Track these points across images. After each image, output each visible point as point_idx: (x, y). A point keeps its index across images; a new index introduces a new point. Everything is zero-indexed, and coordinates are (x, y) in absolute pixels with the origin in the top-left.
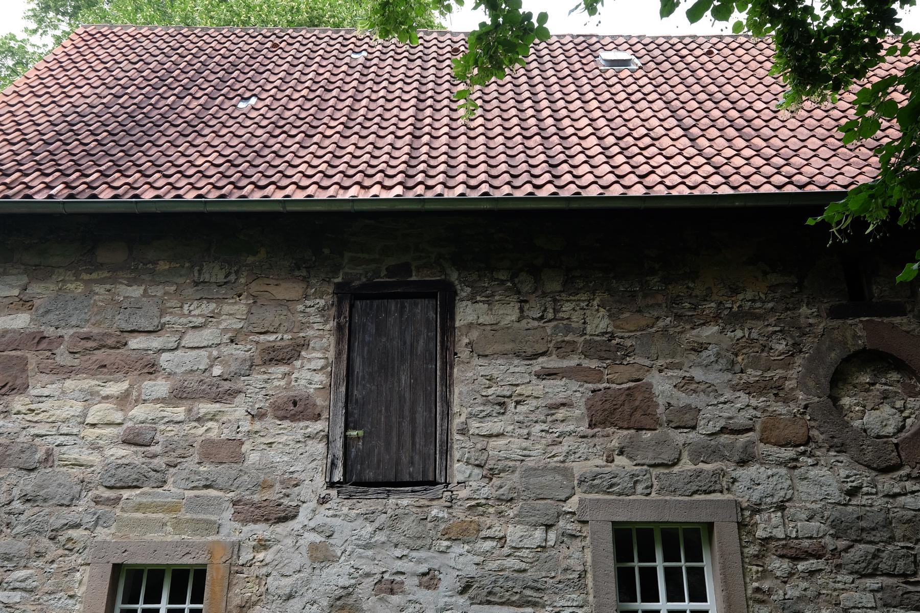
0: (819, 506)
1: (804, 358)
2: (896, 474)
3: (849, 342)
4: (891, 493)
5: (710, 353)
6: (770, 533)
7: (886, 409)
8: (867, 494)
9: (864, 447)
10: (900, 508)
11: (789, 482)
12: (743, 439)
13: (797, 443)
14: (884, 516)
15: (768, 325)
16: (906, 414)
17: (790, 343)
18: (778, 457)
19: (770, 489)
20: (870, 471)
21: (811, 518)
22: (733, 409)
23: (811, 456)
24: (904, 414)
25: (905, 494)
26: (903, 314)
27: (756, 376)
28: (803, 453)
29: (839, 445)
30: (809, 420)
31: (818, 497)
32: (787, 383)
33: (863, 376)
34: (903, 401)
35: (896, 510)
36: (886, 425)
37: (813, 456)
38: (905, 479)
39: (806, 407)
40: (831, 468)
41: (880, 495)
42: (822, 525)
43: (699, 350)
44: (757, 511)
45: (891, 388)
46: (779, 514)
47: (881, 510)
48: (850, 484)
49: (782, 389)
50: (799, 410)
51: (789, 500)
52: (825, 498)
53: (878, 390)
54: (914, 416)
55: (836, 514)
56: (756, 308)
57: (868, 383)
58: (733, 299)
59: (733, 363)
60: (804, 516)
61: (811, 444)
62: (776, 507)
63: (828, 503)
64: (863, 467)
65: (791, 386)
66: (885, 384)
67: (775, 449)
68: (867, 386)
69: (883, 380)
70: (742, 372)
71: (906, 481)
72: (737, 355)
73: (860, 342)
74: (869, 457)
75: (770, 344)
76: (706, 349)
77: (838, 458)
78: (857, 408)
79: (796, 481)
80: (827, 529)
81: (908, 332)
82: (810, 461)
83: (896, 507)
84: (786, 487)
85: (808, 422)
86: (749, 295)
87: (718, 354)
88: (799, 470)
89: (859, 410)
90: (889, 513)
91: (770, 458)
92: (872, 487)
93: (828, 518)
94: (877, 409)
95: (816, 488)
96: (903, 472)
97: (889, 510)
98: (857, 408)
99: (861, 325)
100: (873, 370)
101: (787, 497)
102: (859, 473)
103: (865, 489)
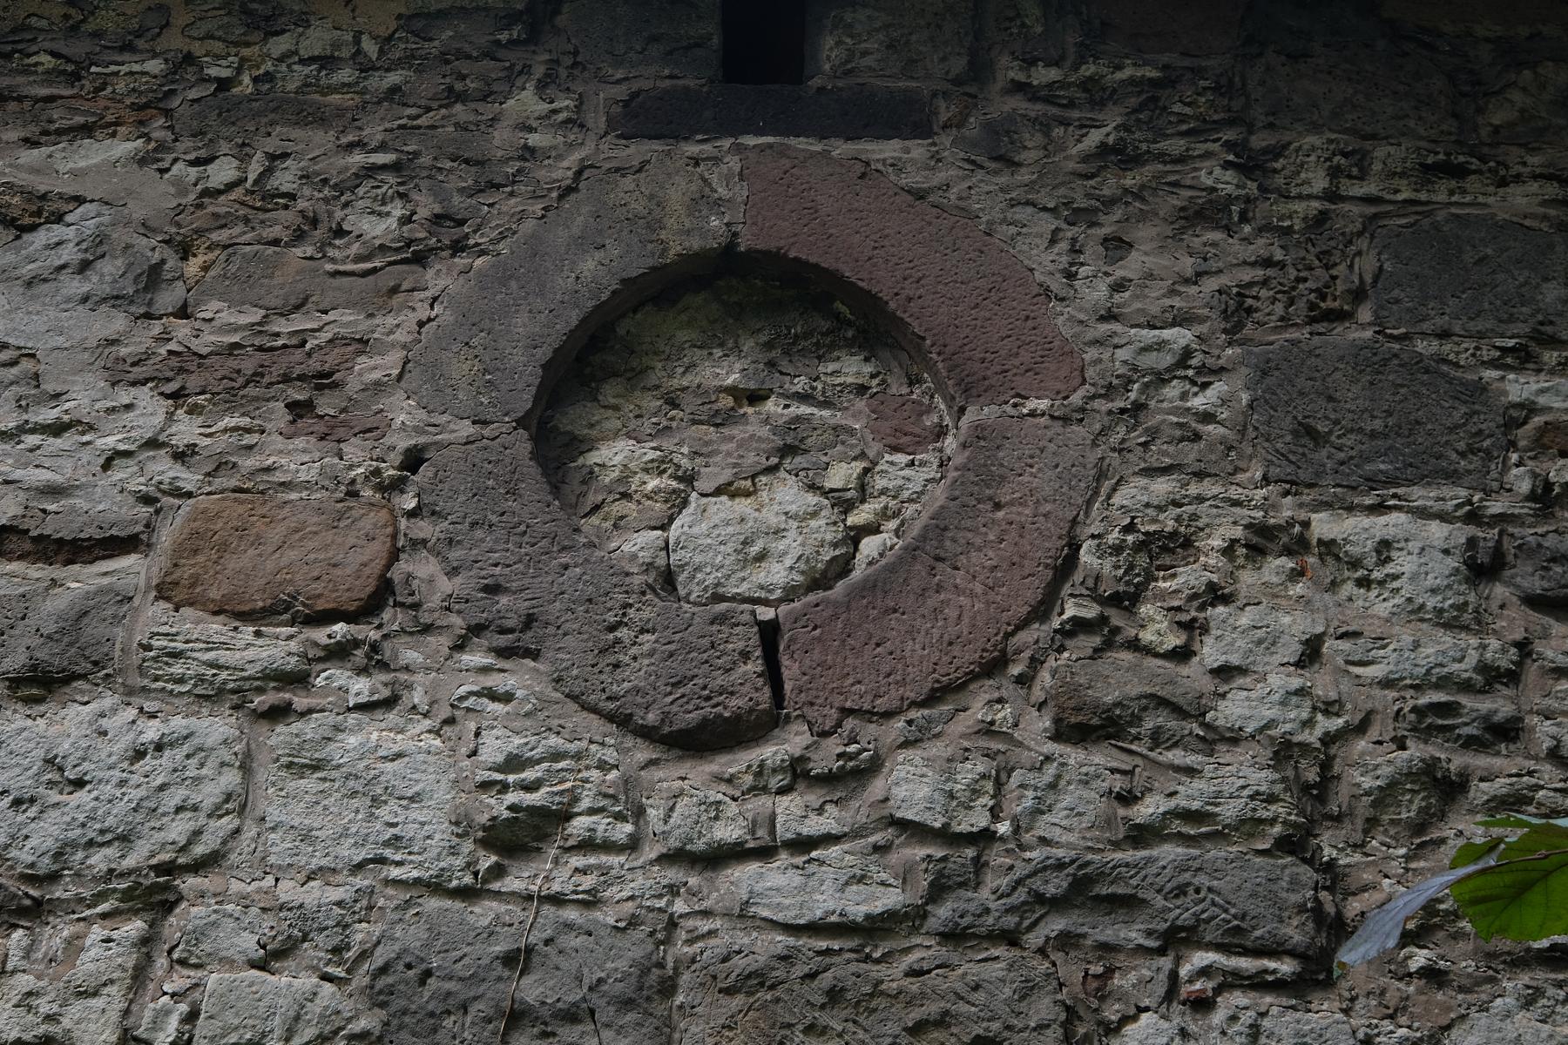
0: (335, 894)
1: (467, 271)
2: (738, 762)
3: (671, 222)
4: (699, 845)
5: (70, 233)
6: (50, 1018)
7: (787, 494)
8: (588, 845)
9: (623, 633)
10: (727, 915)
11: (231, 778)
12: (82, 580)
13: (321, 605)
14: (638, 953)
15: (351, 147)
16: (861, 516)
17: (423, 213)
18: (212, 665)
19: (120, 807)
20: (629, 742)
21: (281, 954)
22: (85, 455)
23: (375, 661)
24: (858, 517)
25: (765, 853)
26: (921, 129)
27: (236, 329)
28: (338, 653)
29: (510, 623)
30: (412, 514)
31: (351, 852)
32: (363, 362)
33: (717, 363)
34: (859, 466)
35: (704, 926)
36: (761, 557)
37: (384, 666)
38: (775, 782)
39: (413, 460)
40: (450, 721)
41: (650, 852)
42: (328, 988)
43: (27, 221)
44: (22, 912)
45: (826, 413)
46: (135, 927)
47: (633, 922)
48: (512, 797)
49: (335, 385)
50: (377, 472)
51: (211, 862)
52: (381, 860)
53: (766, 421)
54: (892, 525)
55: (411, 936)
56: (332, 90)
57: (732, 391)
58: (246, 52)
59: (153, 277)
60: (248, 943)
61: (387, 615)
62: (127, 895)
63: (388, 882)
64: (595, 721)
65: (376, 375)
66: (804, 398)
67: (216, 628)
68: (728, 401)
69: (800, 384)
70: (183, 312)
71: (782, 791)
72: (185, 252)
73: (715, 222)
74: (634, 676)
75: (339, 214)
76: (58, 218)
77: (493, 681)
78: (653, 483)
79: (265, 773)
80: (347, 1007)
81: (920, 195)
82: (362, 688)
83: (706, 914)
84: (208, 804)
85: (403, 523)
86: (316, 41)
87: (100, 239)
88: (296, 727)
89: (656, 491)
90: (667, 941)
91: (177, 669)
92: (620, 817)
93: (364, 955)
94: (747, 494)
95: (351, 814)
96: (771, 752)
97: (672, 924)
98: (653, 483)
99: (734, 163)
100: (769, 346)
101: (199, 850)
102: (573, 747)
103: (579, 825)
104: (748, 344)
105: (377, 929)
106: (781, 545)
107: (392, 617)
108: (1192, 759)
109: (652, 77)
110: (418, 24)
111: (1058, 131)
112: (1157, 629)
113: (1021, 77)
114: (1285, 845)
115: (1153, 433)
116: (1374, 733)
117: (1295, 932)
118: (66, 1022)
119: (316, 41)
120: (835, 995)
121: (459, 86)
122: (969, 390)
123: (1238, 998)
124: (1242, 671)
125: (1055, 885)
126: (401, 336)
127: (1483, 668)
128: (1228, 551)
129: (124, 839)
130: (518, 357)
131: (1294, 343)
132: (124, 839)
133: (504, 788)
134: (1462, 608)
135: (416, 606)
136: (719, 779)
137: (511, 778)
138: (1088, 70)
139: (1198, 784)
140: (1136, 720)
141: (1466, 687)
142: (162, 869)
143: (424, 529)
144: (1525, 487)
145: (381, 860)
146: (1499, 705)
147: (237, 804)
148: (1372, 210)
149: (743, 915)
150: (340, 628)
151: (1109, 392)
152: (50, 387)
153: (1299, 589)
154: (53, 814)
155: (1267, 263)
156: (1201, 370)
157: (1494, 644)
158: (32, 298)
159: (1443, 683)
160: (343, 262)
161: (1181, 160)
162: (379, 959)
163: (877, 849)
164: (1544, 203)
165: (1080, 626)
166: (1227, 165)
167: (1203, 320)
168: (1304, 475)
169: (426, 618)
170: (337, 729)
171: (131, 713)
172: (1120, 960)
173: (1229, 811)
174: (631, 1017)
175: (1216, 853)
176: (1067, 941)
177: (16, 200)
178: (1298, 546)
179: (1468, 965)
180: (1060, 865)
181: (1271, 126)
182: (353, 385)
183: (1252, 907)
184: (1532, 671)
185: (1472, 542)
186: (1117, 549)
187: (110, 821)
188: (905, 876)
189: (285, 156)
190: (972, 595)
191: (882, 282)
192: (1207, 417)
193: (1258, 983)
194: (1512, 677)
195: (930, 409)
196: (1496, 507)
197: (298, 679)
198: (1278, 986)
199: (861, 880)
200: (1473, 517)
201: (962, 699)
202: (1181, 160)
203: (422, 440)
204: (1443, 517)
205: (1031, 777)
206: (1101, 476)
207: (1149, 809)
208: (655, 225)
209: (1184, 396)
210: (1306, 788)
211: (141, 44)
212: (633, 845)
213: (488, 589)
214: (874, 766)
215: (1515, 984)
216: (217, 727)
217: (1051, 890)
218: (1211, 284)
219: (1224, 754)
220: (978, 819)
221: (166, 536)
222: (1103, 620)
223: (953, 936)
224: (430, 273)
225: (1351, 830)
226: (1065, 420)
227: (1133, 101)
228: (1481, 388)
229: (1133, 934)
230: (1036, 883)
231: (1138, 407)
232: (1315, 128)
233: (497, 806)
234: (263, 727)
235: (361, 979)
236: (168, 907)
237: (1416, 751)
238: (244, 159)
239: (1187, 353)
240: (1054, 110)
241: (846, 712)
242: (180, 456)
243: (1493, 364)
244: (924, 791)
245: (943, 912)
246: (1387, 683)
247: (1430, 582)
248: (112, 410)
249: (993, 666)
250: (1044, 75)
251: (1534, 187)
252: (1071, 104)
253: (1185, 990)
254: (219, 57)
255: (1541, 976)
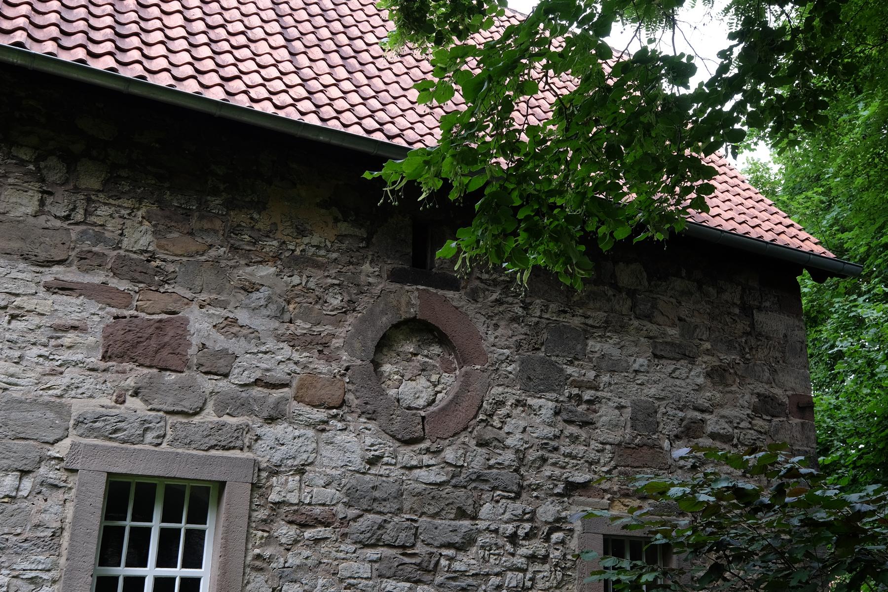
0: (339, 472)
2: (417, 447)
3: (402, 309)
5: (261, 295)
6: (284, 497)
7: (422, 382)
8: (387, 464)
9: (394, 416)
10: (414, 480)
11: (314, 445)
12: (277, 394)
14: (397, 487)
16: (438, 388)
17: (346, 299)
19: (293, 451)
20: (394, 441)
21: (328, 485)
23: (342, 420)
25: (421, 468)
26: (457, 289)
27: (305, 329)
28: (334, 417)
29: (371, 412)
30: (348, 383)
32: (334, 341)
34: (438, 376)
35: (409, 482)
37: (344, 420)
38: (424, 452)
39: (347, 369)
40: (358, 434)
41: (399, 466)
43: (250, 290)
44: (275, 473)
45: (431, 361)
46: (297, 478)
48: (373, 453)
50: (340, 371)
52: (346, 465)
54: (445, 391)
55: (354, 482)
56: (320, 256)
57: (411, 353)
59: (283, 311)
60: (322, 482)
61: (344, 408)
62: (296, 471)
63: (348, 470)
64: (388, 436)
65: (337, 345)
66: (427, 356)
67: (308, 408)
69: (426, 352)
75: (326, 297)
76: (258, 290)
77: (367, 425)
78: (396, 377)
79: (322, 444)
81: (457, 308)
82: (340, 425)
83: (409, 480)
84: (310, 451)
85: (346, 385)
86: (315, 240)
87: (270, 298)
88: (327, 433)
91: (301, 418)
92: (393, 458)
93: (345, 486)
96: (423, 446)
98: (396, 377)
100: (419, 341)
101: (309, 461)
103: (385, 459)
104: (414, 340)
105: (347, 480)
106: (422, 395)
107: (344, 408)
108: (501, 452)
109: (398, 265)
110: (340, 238)
111: (487, 293)
112: (496, 423)
113: (480, 276)
114: (515, 471)
115: (500, 375)
116: (533, 448)
117: (515, 488)
118: (288, 498)
119: (315, 240)
120: (433, 498)
121: (351, 260)
122: (464, 361)
123: (504, 501)
124: (511, 433)
125: (474, 477)
126: (343, 335)
127: (554, 435)
128: (511, 406)
129: (294, 458)
130: (370, 344)
131: (529, 356)
132: (294, 458)
133: (371, 450)
134: (552, 422)
135: (350, 406)
136: (412, 451)
137: (372, 448)
138: (494, 276)
139: (501, 457)
140: (491, 443)
141: (551, 439)
142: (303, 465)
143: (350, 387)
144: (567, 395)
145: (346, 465)
146: (555, 443)
147: (316, 451)
148: (548, 322)
149: (416, 481)
150: (334, 410)
151: (492, 365)
152: (263, 341)
153: (523, 415)
154: (279, 451)
155: (526, 334)
156: (510, 361)
157: (557, 430)
158: (255, 314)
159: (547, 438)
160: (327, 311)
161: (511, 304)
162: (348, 486)
163: (442, 468)
164: (581, 323)
165: (482, 420)
166: (521, 307)
167: (512, 348)
168: (527, 389)
169: (352, 410)
170: (335, 435)
171: (291, 428)
172: (484, 492)
173: (506, 463)
174: (396, 500)
175: (503, 471)
176: (475, 488)
177: (247, 284)
178: (524, 405)
179: (543, 496)
180: (475, 473)
181: (530, 296)
182: (332, 347)
183: (508, 483)
184: (563, 436)
185: (556, 407)
186: (491, 404)
187: (291, 454)
188: (447, 474)
189: (311, 277)
190: (463, 412)
191: (448, 331)
192: (510, 373)
193: (508, 498)
194: (559, 437)
195: (453, 363)
196: (561, 399)
197: (326, 422)
198: (511, 499)
199: (439, 474)
200: (557, 401)
201: (459, 436)
202: (511, 304)
203: (350, 364)
204: (552, 401)
205: (471, 454)
206: (489, 386)
207: (492, 462)
208: (399, 309)
209: (506, 367)
210: (520, 459)
211: (271, 235)
212: (395, 464)
213: (365, 403)
214: (442, 450)
215: (550, 499)
216: (310, 433)
217: (473, 478)
218: (515, 338)
219: (507, 451)
220: (460, 463)
221: (295, 384)
222: (487, 419)
223: (455, 486)
224: (348, 317)
225: (526, 468)
226: (483, 371)
227: (503, 286)
228: (562, 370)
229: (487, 487)
230: (471, 476)
231: (498, 369)
232: (539, 298)
233: (370, 455)
234: (320, 433)
235: (344, 490)
236: (303, 473)
237: (540, 453)
238: (301, 276)
239: (508, 356)
240: (486, 287)
241: (438, 438)
242: (296, 363)
243: (566, 364)
244: (452, 456)
245: (454, 481)
246: (537, 438)
247: (548, 416)
248: (278, 349)
249: (465, 429)
250: (485, 276)
251: (579, 318)
252: (489, 285)
253: (495, 499)
254: (291, 242)
255: (555, 498)
